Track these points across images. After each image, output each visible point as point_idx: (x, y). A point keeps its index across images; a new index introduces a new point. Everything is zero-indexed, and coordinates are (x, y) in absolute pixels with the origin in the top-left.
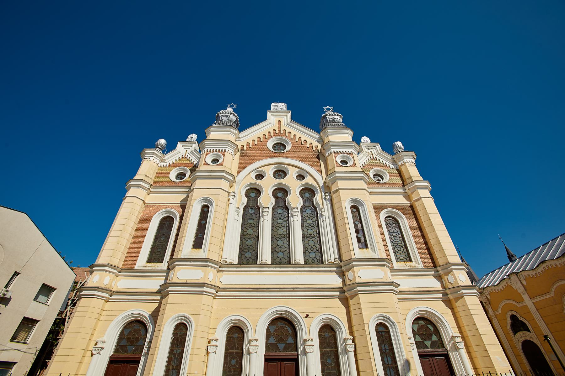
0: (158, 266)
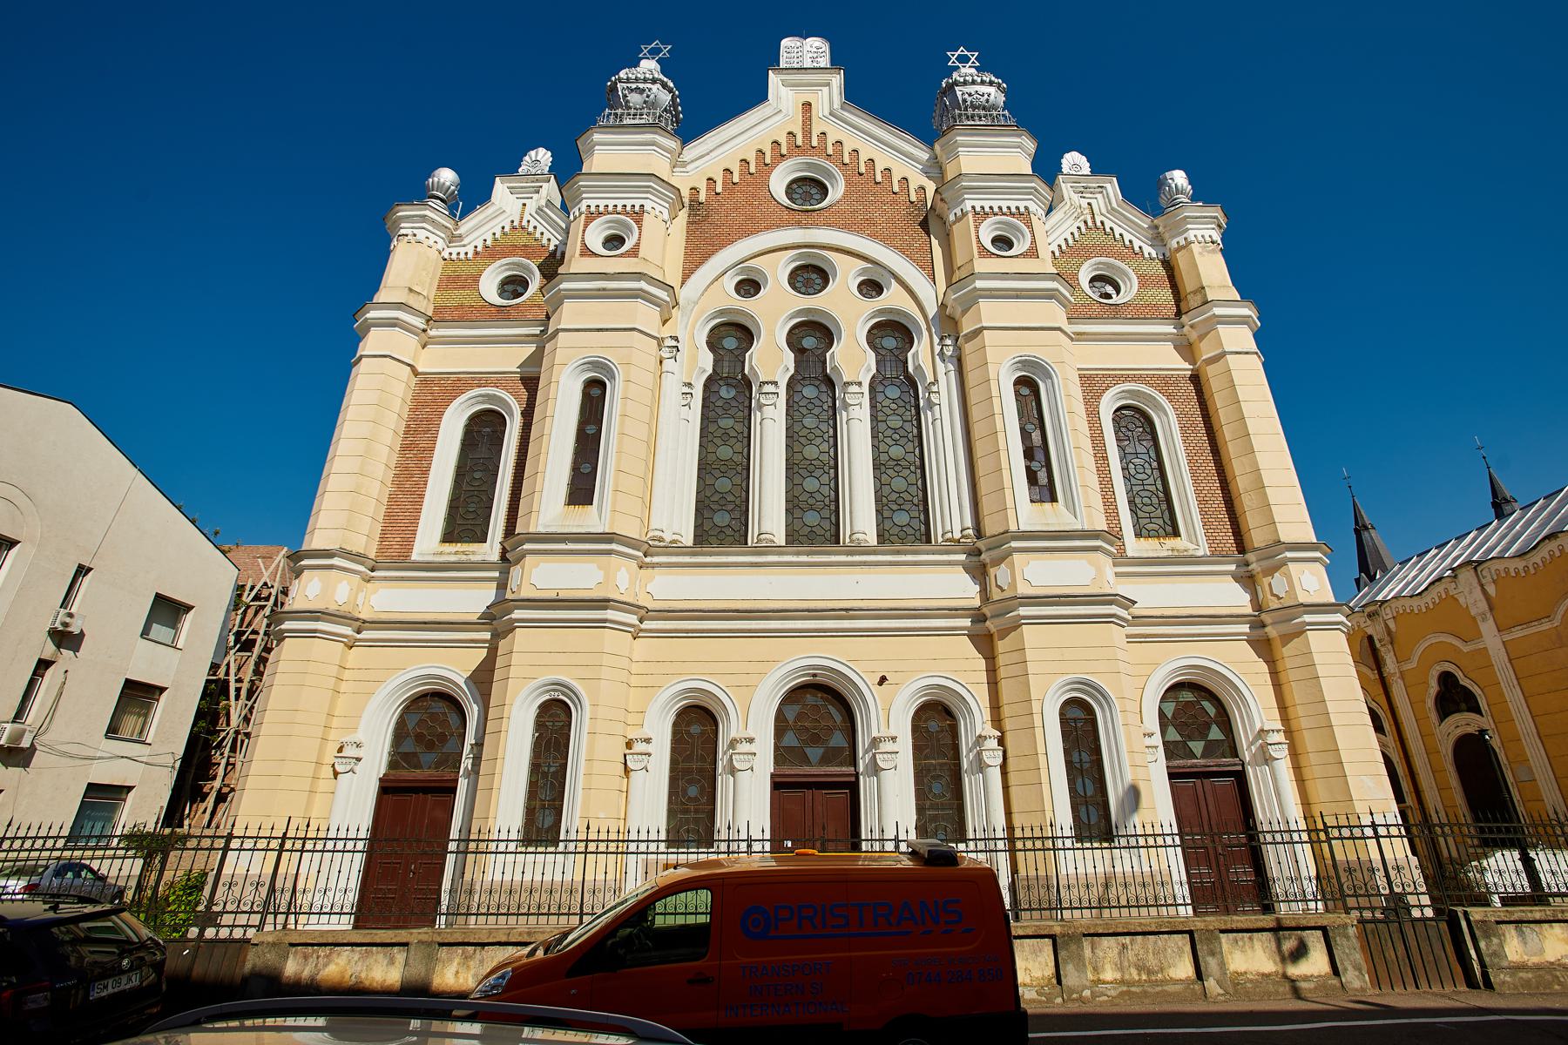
0: (474, 553)
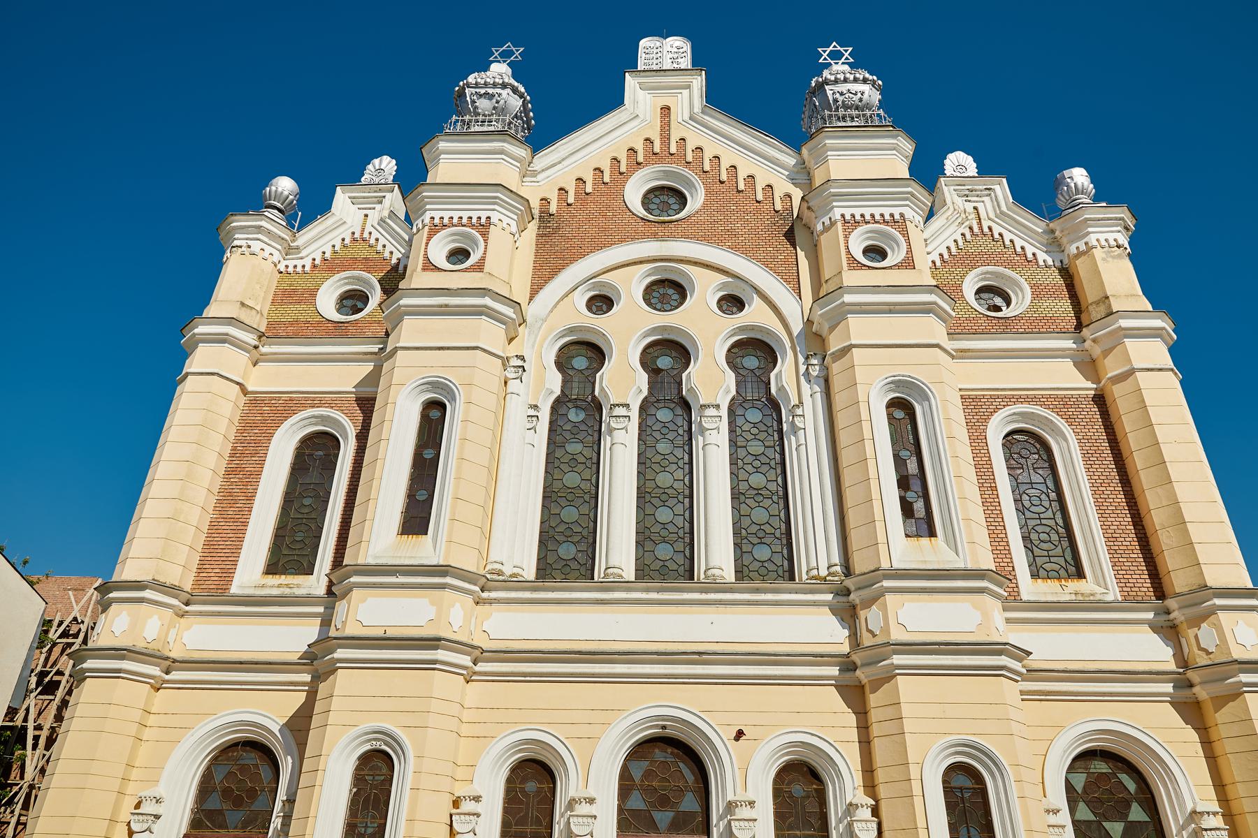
0: (298, 586)
